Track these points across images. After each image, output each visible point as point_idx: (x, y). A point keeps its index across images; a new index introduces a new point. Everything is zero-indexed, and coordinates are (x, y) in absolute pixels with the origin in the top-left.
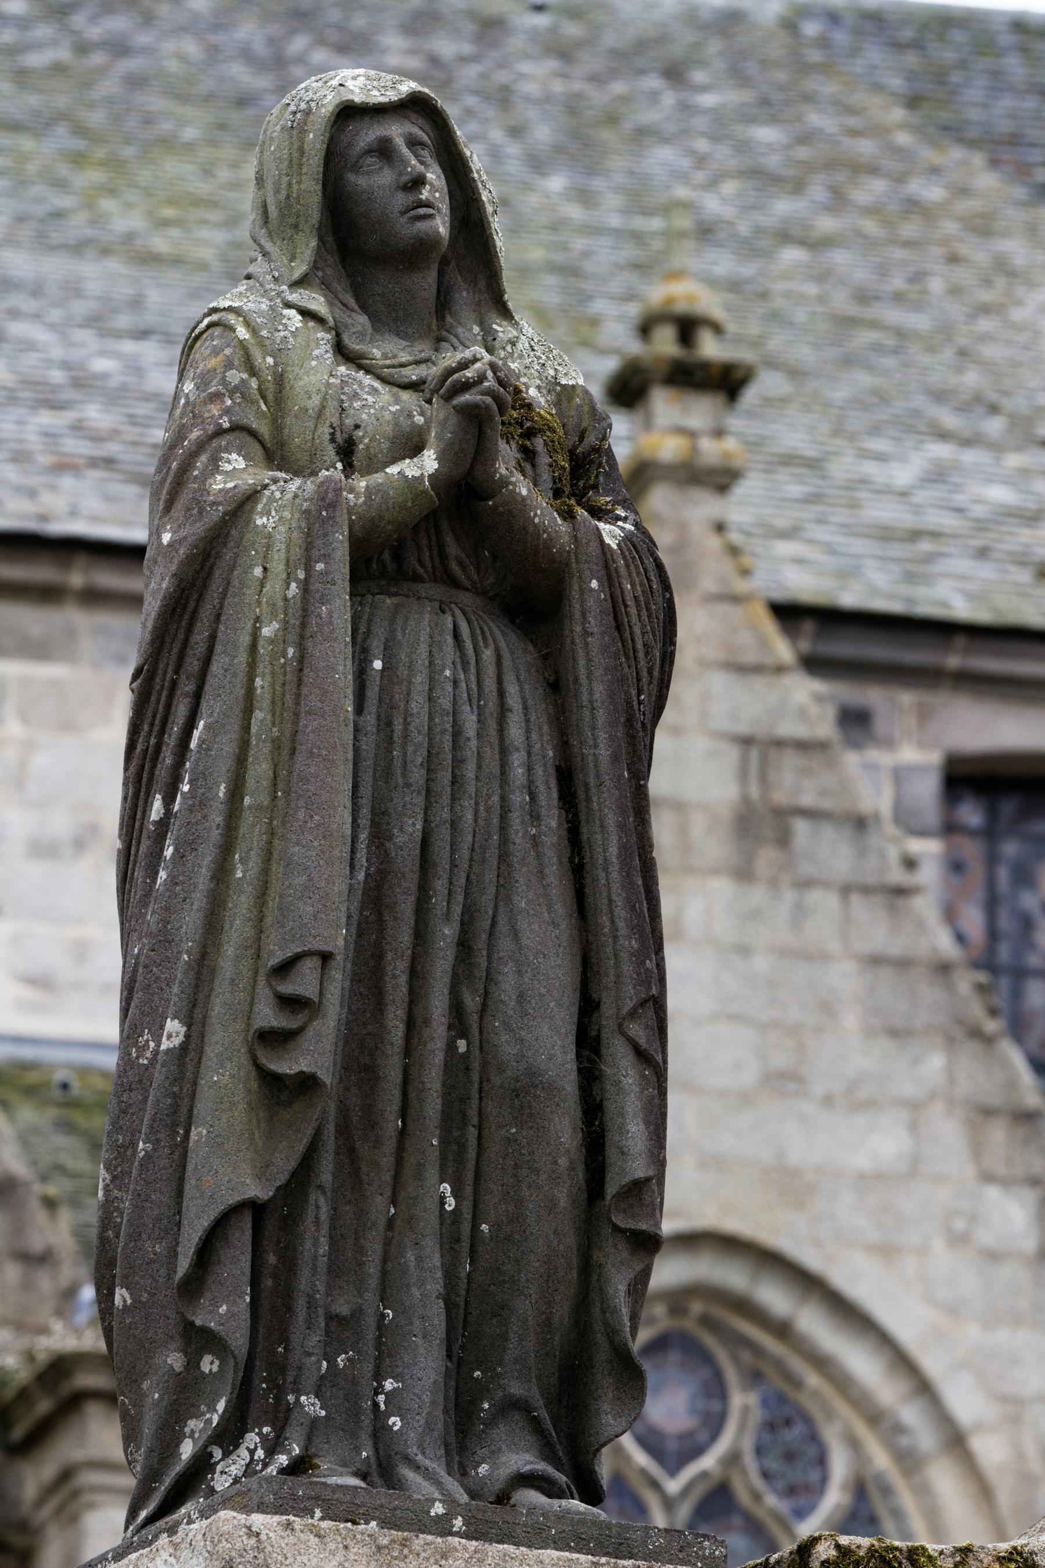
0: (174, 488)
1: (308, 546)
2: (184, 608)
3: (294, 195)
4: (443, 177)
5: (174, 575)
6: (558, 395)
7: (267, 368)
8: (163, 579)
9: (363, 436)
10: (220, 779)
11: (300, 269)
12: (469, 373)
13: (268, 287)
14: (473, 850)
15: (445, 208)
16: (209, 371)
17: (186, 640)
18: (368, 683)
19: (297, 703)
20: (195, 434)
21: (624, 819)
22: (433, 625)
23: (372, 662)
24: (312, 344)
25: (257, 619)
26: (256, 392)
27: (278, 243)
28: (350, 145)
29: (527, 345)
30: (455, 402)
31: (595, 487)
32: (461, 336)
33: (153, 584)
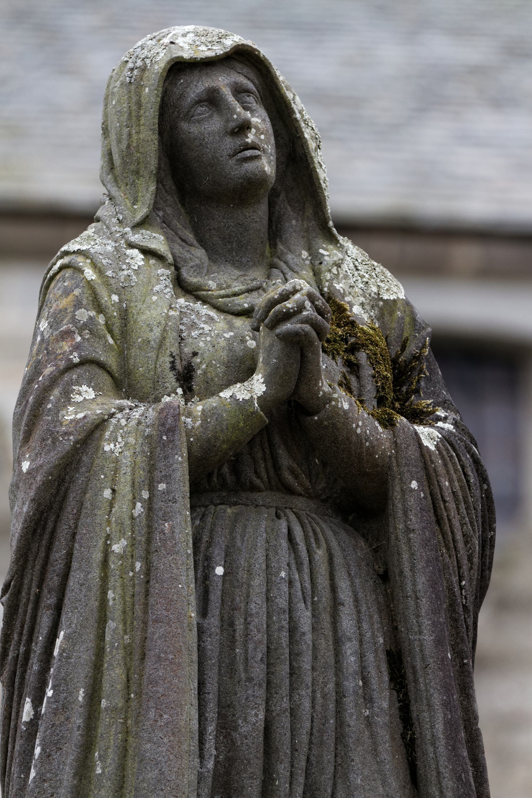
0: (31, 420)
1: (152, 469)
2: (44, 528)
3: (134, 145)
4: (268, 119)
5: (33, 500)
6: (381, 309)
7: (113, 305)
8: (24, 504)
9: (201, 362)
10: (79, 684)
11: (142, 211)
12: (289, 304)
13: (113, 229)
14: (311, 734)
15: (270, 148)
16: (61, 311)
17: (47, 557)
18: (211, 588)
19: (145, 612)
20: (48, 370)
21: (448, 697)
22: (269, 530)
23: (214, 569)
24: (154, 280)
25: (108, 537)
26: (103, 327)
27: (123, 188)
28: (182, 96)
29: (352, 265)
30: (278, 331)
31: (417, 391)
32: (291, 262)
33: (16, 508)
